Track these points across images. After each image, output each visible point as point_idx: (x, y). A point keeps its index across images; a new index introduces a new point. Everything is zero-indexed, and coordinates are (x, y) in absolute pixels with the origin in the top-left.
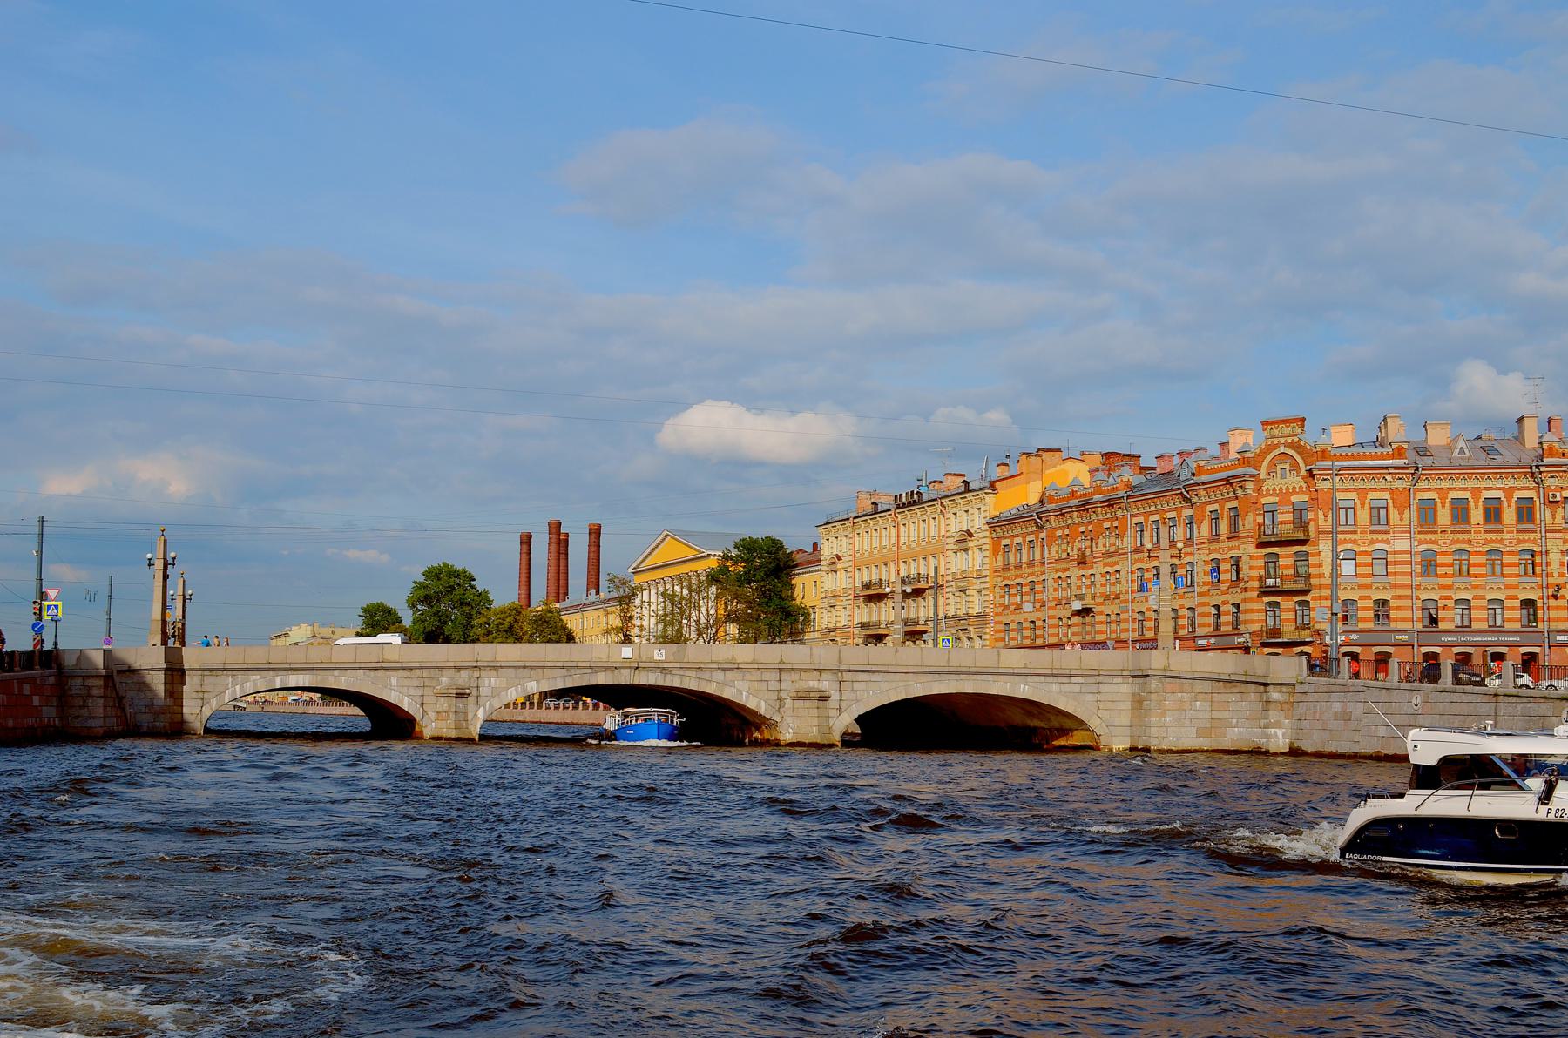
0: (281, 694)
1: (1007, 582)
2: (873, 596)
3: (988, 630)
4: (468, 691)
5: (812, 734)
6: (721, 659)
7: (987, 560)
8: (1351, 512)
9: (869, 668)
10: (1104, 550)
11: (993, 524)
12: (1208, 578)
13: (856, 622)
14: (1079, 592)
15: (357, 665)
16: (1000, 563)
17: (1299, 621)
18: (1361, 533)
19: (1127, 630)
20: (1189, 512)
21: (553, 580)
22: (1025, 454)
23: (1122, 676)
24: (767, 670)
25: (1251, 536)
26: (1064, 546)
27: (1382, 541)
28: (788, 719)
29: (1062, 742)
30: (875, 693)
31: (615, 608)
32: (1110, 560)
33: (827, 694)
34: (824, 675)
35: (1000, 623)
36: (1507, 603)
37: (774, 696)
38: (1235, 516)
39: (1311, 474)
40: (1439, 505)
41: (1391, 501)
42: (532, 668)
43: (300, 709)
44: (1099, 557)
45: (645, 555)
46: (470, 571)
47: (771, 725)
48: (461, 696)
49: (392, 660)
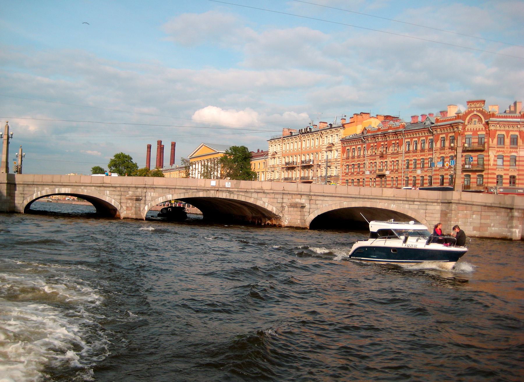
0: (64, 196)
1: (348, 164)
2: (290, 167)
3: (339, 182)
4: (141, 198)
5: (298, 223)
6: (256, 188)
7: (340, 155)
9: (324, 194)
10: (391, 152)
11: (343, 141)
14: (380, 168)
15: (92, 185)
16: (345, 156)
17: (478, 183)
18: (506, 148)
20: (431, 137)
22: (356, 114)
23: (437, 202)
24: (277, 193)
26: (374, 150)
27: (515, 152)
28: (286, 216)
31: (184, 170)
32: (394, 156)
33: (304, 205)
34: (303, 197)
35: (344, 179)
37: (280, 205)
39: (487, 123)
42: (170, 189)
43: (70, 202)
44: (389, 155)
46: (131, 156)
47: (277, 218)
48: (138, 200)
49: (107, 183)
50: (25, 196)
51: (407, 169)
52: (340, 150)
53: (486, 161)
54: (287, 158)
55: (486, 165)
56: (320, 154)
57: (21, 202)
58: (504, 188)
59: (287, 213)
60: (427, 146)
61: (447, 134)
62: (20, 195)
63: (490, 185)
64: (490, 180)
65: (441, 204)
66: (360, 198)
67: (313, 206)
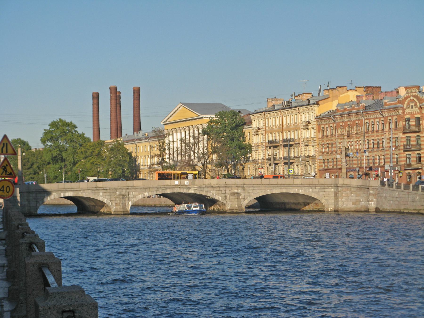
1: (323, 143)
4: (125, 196)
7: (316, 134)
9: (253, 186)
15: (88, 189)
16: (321, 135)
19: (364, 163)
21: (114, 121)
24: (221, 187)
25: (401, 130)
28: (229, 202)
29: (307, 208)
30: (255, 194)
44: (354, 135)
45: (170, 115)
46: (74, 123)
50: (38, 200)
52: (315, 128)
57: (35, 205)
59: (229, 200)
62: (34, 200)
65: (334, 187)
66: (278, 187)
67: (246, 194)
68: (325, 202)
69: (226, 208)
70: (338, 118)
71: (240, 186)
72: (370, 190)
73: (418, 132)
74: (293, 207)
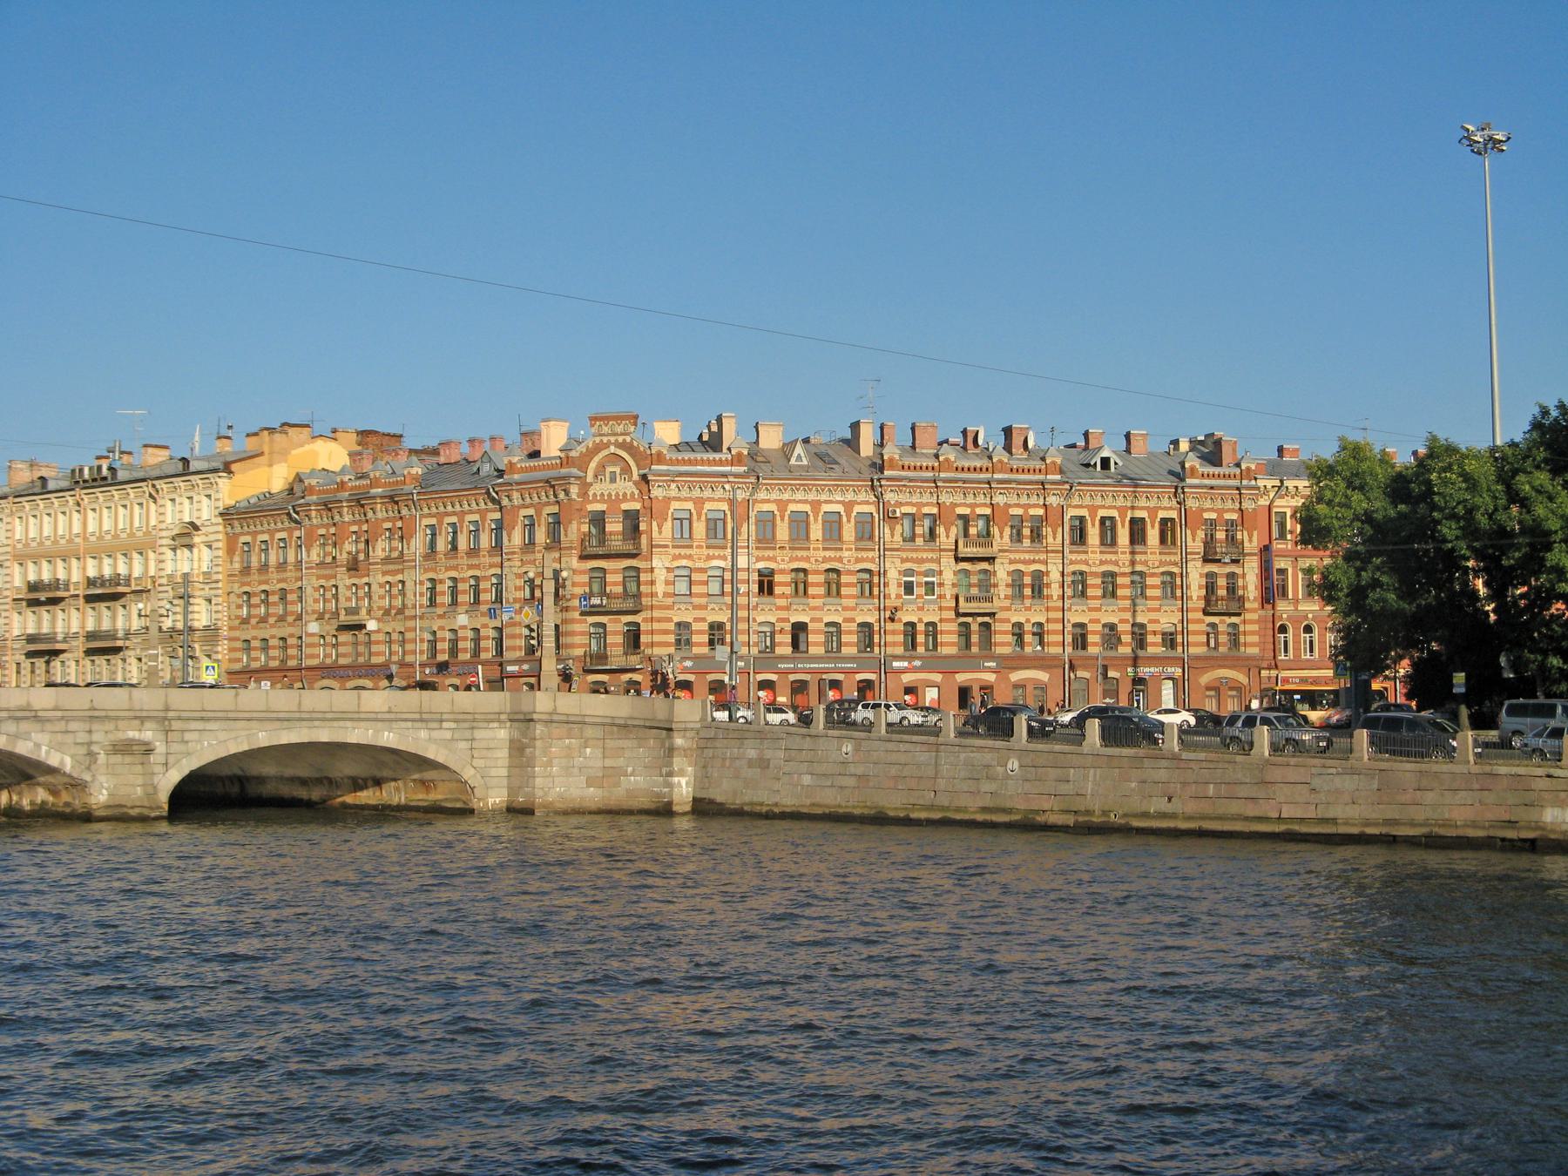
1: (246, 589)
8: (686, 523)
11: (227, 515)
12: (520, 595)
13: (16, 632)
14: (348, 605)
16: (237, 566)
24: (74, 719)
28: (102, 779)
32: (391, 567)
34: (148, 725)
35: (236, 639)
36: (845, 626)
37: (83, 750)
38: (556, 524)
39: (644, 478)
40: (778, 518)
41: (728, 513)
44: (377, 563)
51: (431, 605)
52: (220, 545)
53: (646, 583)
54: (31, 566)
55: (647, 596)
56: (151, 555)
58: (696, 658)
60: (485, 541)
61: (539, 508)
63: (657, 651)
64: (657, 638)
65: (508, 724)
67: (175, 747)
68: (475, 776)
69: (93, 801)
70: (313, 514)
71: (152, 714)
72: (675, 734)
73: (634, 556)
74: (287, 791)
